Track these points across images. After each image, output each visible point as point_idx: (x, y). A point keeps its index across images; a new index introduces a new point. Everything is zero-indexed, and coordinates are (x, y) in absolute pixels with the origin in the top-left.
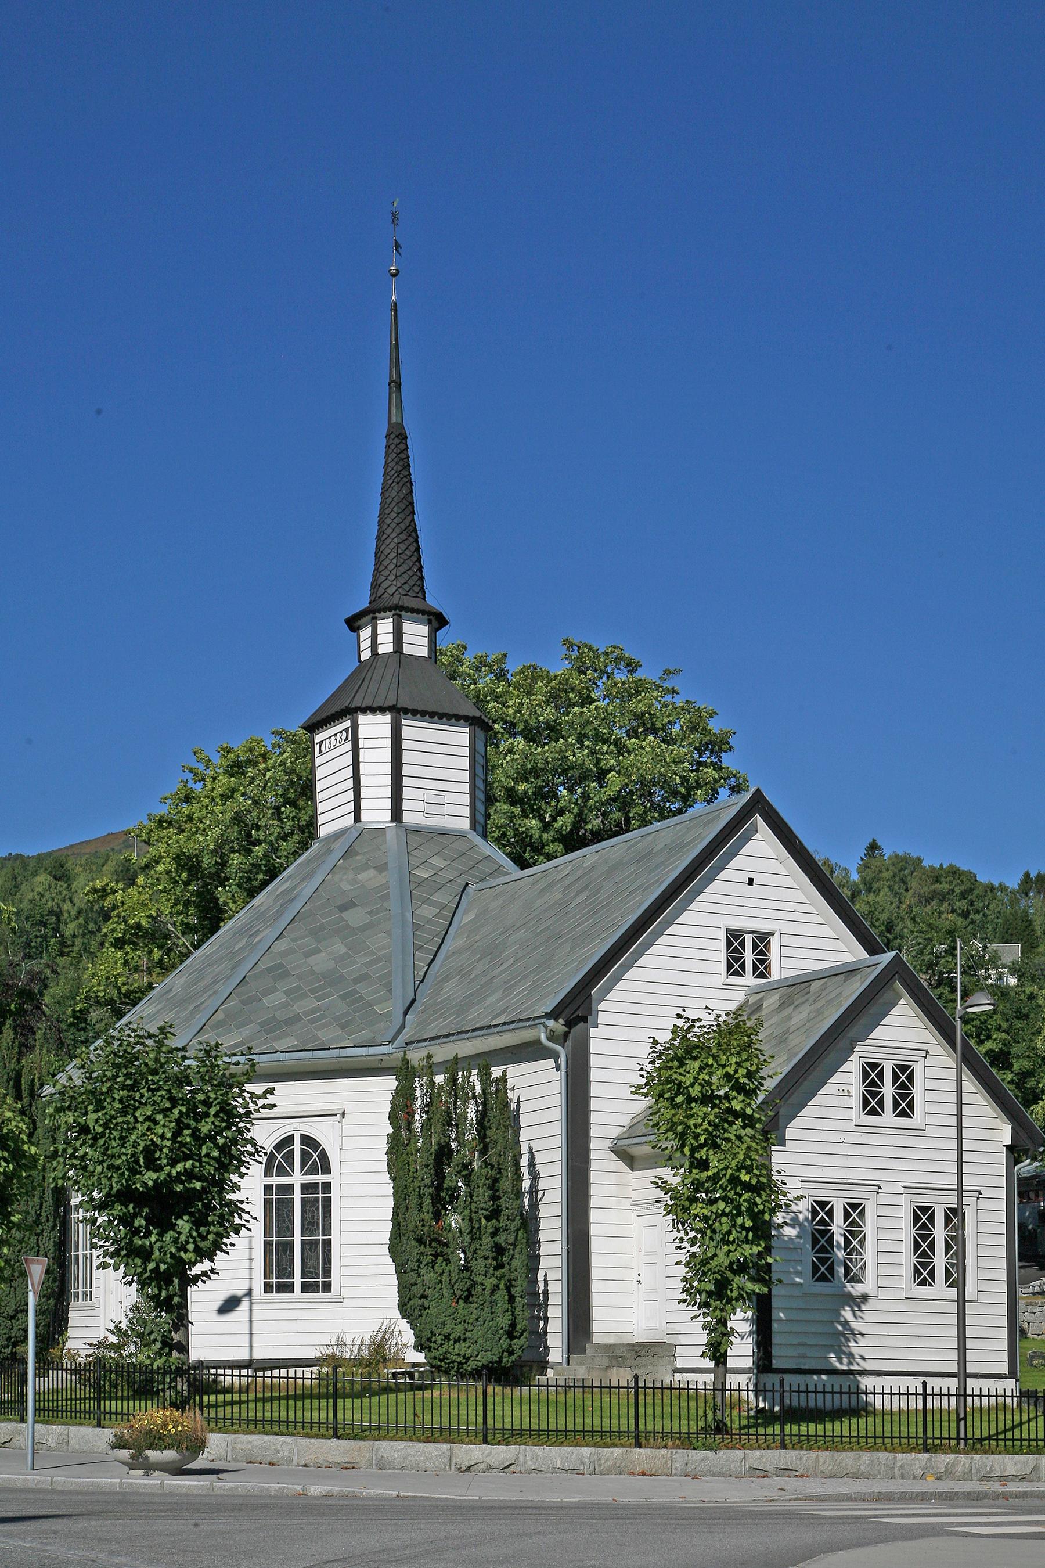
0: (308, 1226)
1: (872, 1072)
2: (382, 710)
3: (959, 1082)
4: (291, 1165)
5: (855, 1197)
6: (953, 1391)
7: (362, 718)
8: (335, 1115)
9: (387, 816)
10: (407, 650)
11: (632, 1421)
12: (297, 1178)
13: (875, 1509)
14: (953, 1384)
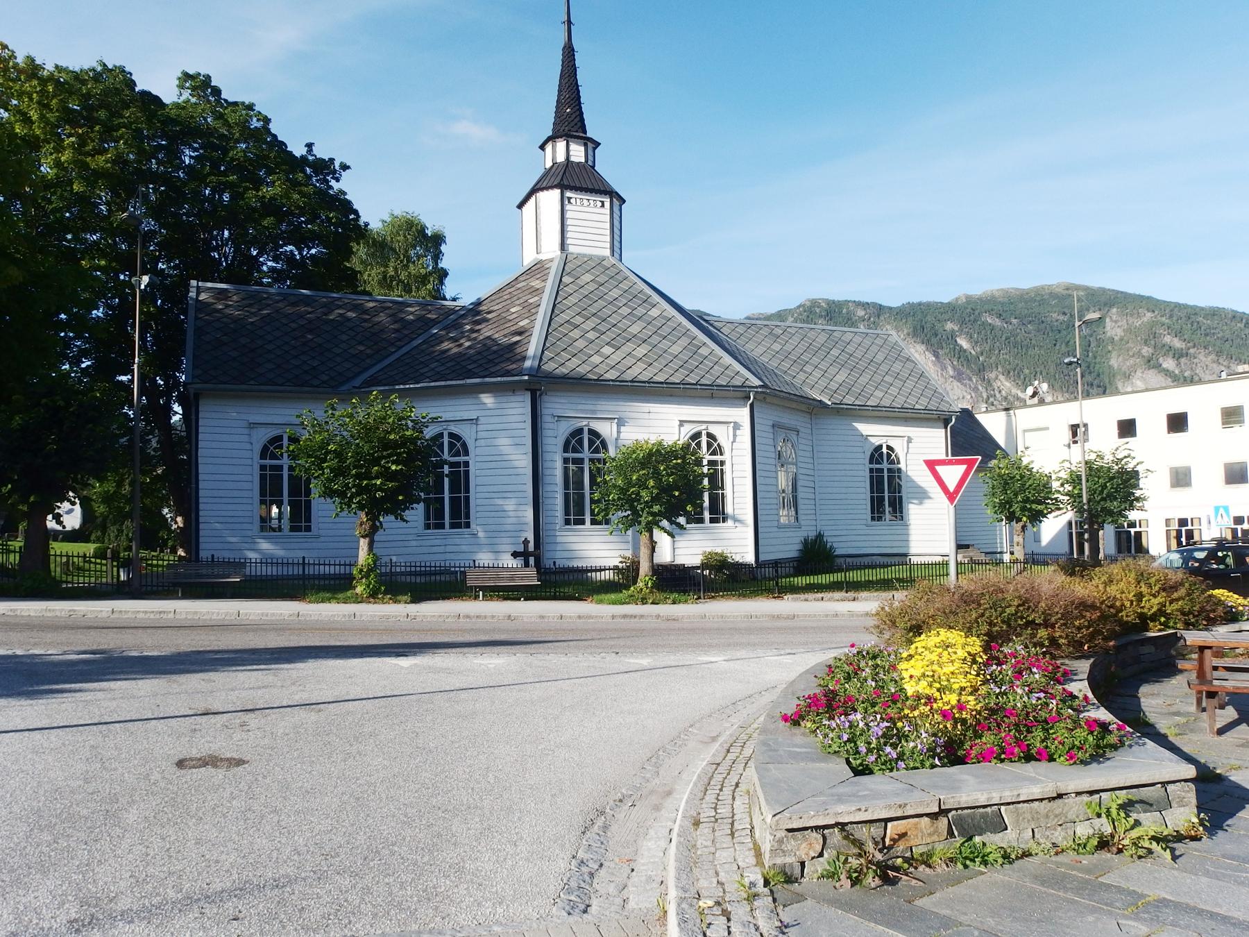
12: (885, 466)
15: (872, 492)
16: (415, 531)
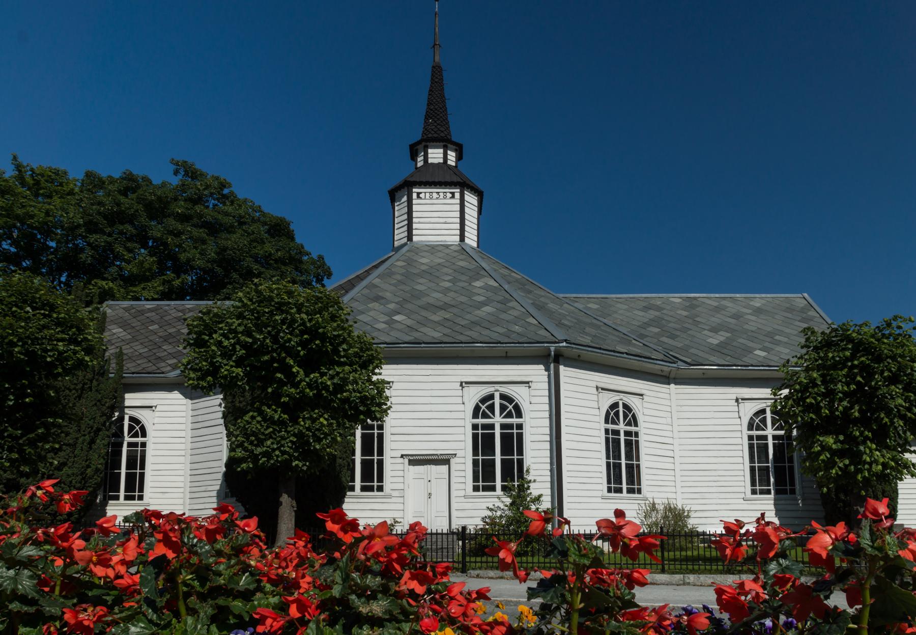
0: (629, 456)
4: (766, 426)
12: (498, 420)
15: (608, 457)
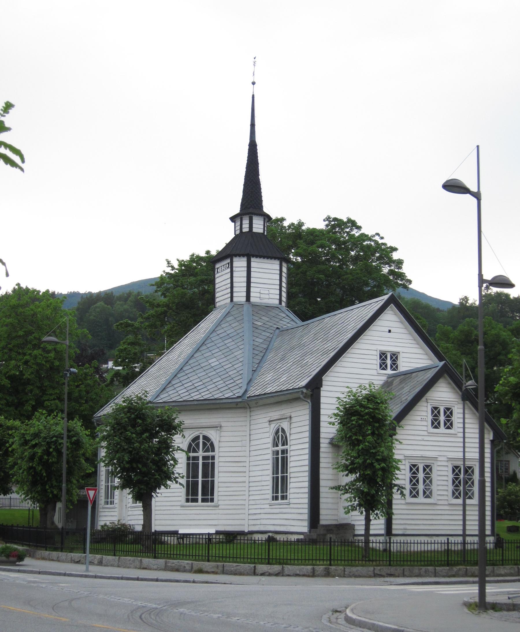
0: (205, 475)
1: (435, 411)
2: (243, 256)
3: (464, 413)
5: (428, 462)
6: (492, 542)
7: (235, 259)
8: (217, 427)
9: (244, 299)
10: (255, 230)
11: (329, 556)
12: (201, 454)
13: (463, 590)
14: (460, 539)
16: (180, 503)
